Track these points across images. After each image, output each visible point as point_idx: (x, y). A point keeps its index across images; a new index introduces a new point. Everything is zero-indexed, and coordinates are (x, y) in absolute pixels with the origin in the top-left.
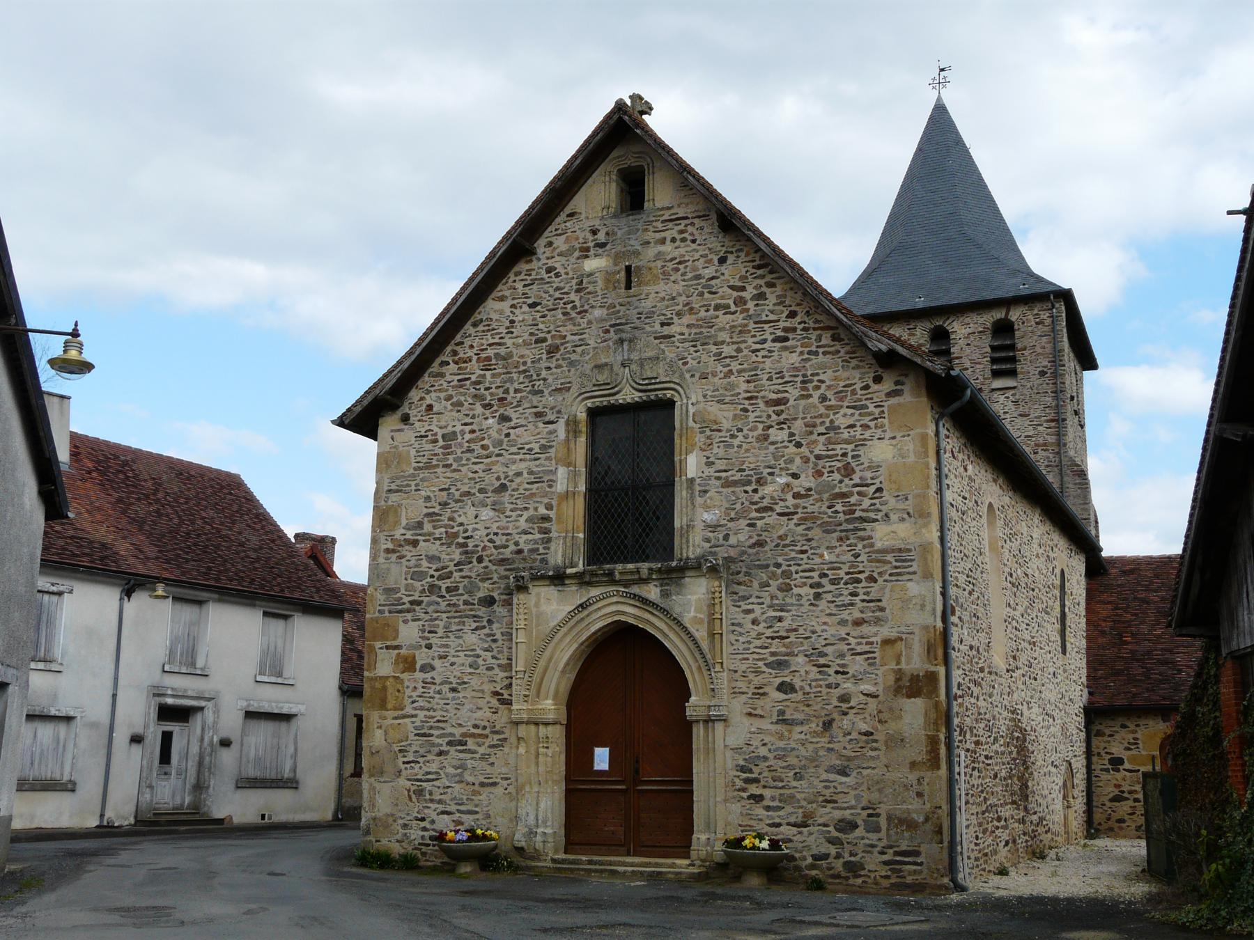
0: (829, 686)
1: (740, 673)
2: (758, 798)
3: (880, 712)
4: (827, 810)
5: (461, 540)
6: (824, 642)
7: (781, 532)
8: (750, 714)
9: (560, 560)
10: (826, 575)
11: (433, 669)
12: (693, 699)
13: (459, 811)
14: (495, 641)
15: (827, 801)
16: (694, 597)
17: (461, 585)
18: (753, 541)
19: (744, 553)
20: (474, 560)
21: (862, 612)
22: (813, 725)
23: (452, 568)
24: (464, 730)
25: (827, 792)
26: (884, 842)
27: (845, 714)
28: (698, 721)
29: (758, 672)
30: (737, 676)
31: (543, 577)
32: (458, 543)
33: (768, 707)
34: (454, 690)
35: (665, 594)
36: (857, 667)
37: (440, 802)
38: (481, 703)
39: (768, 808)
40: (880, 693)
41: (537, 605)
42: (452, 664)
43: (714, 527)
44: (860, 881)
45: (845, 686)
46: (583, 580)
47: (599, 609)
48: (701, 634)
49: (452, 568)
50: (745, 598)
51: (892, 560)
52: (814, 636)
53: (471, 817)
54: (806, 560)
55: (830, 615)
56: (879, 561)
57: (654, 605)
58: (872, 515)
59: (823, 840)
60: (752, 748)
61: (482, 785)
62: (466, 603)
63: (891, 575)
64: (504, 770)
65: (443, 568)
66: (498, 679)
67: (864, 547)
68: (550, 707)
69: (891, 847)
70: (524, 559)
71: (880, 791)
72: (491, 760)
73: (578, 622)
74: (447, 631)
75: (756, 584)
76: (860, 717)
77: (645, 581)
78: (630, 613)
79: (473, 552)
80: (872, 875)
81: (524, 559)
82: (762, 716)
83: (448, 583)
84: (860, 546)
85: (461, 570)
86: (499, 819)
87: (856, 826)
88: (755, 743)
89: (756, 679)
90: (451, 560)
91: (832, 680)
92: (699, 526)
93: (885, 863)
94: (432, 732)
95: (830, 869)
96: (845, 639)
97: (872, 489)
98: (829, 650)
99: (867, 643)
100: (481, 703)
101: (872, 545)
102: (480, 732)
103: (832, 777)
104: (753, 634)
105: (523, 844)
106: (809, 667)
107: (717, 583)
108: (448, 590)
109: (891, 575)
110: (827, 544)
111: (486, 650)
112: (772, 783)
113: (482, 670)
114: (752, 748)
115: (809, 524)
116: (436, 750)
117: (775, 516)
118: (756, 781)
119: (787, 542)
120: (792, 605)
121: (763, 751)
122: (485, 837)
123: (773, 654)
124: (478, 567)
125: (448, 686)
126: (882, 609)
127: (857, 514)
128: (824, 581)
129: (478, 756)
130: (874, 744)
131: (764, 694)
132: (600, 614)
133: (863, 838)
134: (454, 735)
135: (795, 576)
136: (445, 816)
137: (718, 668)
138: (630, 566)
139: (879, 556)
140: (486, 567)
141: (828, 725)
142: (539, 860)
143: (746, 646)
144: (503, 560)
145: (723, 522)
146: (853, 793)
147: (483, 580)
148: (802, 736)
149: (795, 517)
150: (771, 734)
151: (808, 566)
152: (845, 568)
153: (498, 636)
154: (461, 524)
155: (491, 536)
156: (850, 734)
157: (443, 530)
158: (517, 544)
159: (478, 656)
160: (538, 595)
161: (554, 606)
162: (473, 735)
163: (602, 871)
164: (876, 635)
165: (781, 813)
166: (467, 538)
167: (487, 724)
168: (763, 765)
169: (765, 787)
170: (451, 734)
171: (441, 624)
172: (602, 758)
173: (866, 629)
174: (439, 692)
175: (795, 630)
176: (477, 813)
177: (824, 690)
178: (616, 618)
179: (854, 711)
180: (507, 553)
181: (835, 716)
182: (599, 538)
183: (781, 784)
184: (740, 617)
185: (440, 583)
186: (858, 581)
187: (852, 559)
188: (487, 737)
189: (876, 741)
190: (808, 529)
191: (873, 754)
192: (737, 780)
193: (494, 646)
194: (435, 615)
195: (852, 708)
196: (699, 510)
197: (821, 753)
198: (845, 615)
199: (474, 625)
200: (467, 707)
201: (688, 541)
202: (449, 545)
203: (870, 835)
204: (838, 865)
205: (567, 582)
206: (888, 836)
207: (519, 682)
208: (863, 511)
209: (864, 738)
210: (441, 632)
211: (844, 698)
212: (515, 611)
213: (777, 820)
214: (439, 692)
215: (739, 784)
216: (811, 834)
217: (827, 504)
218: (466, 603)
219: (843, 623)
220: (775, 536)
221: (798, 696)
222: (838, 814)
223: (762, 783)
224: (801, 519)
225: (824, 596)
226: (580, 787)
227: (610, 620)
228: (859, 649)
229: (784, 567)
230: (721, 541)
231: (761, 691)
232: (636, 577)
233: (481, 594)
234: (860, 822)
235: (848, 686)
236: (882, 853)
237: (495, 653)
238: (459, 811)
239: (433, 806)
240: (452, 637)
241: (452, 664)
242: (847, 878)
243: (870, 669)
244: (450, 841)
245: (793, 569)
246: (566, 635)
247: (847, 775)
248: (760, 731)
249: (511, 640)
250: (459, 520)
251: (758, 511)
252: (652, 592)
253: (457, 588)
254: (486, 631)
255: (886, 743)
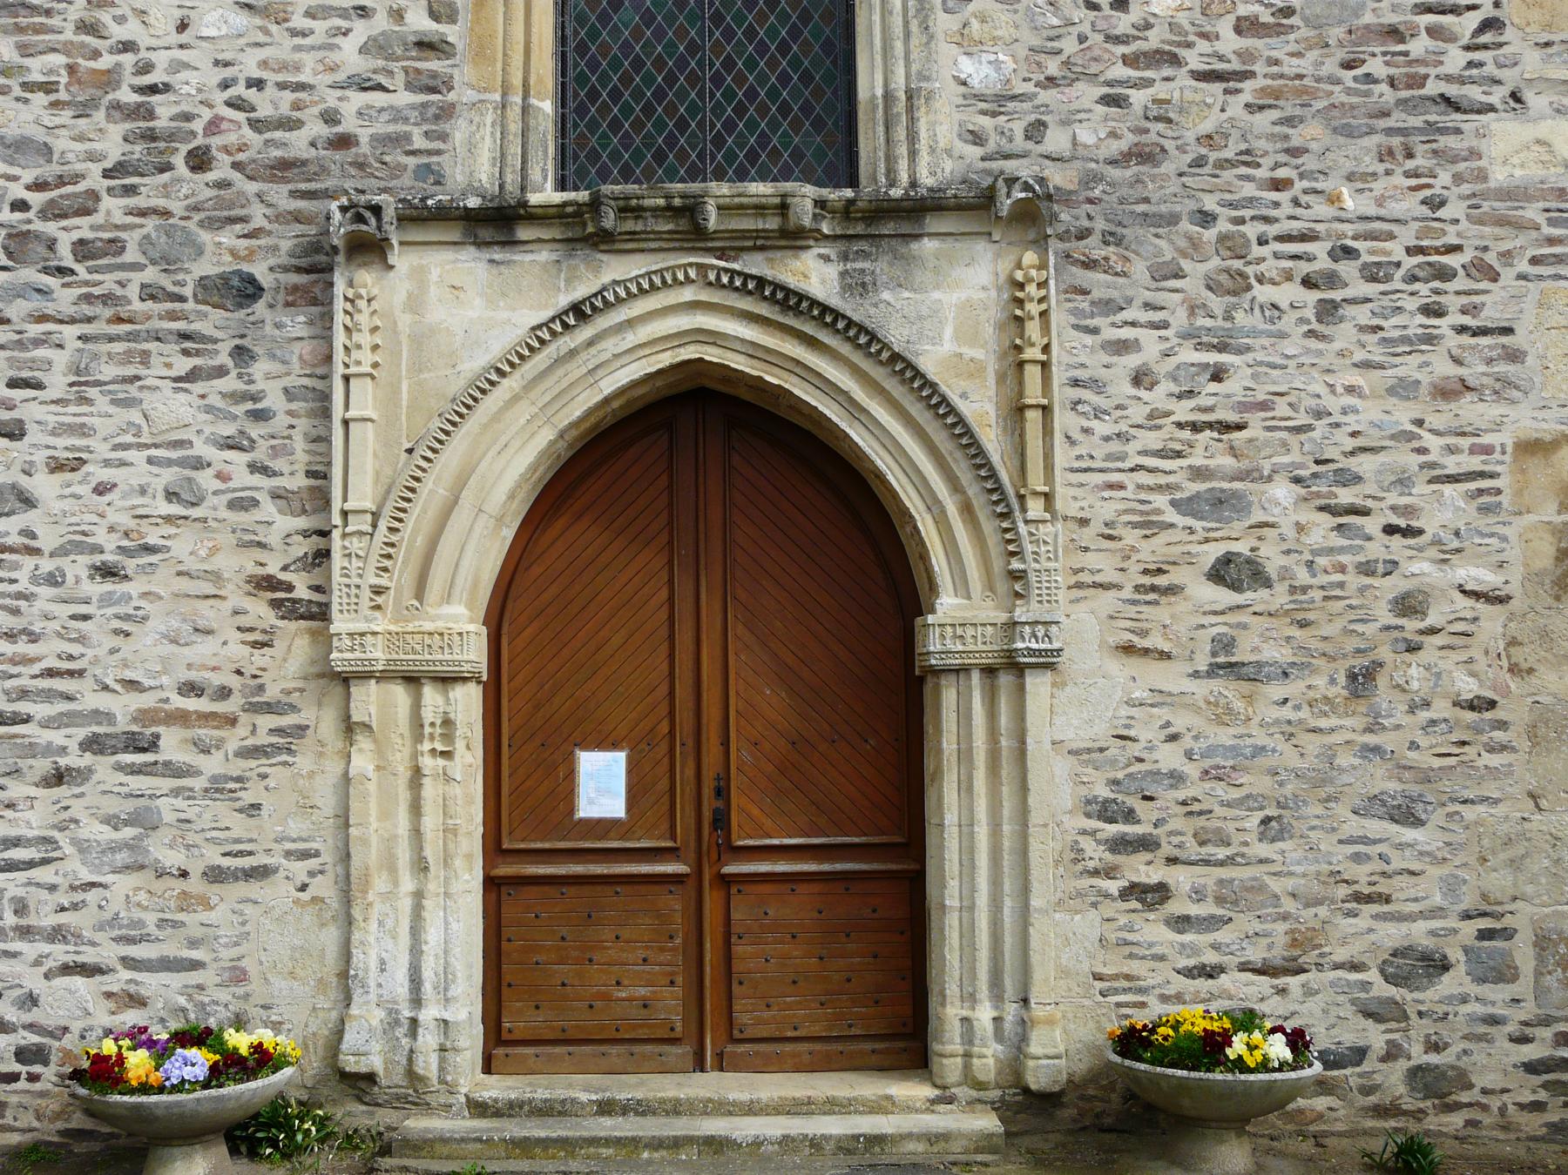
0: (1367, 569)
1: (1096, 527)
2: (1151, 895)
3: (1513, 642)
4: (1362, 923)
5: (127, 96)
6: (1350, 444)
7: (1207, 127)
8: (1128, 649)
9: (485, 174)
10: (1349, 253)
11: (28, 502)
12: (947, 604)
13: (129, 963)
14: (260, 416)
15: (1358, 898)
16: (946, 304)
17: (132, 239)
18: (1123, 145)
19: (1097, 178)
20: (179, 161)
21: (1458, 361)
22: (1320, 681)
23: (94, 180)
24: (147, 701)
25: (1361, 872)
26: (1528, 1010)
27: (1413, 648)
28: (962, 671)
29: (1150, 525)
30: (1087, 536)
31: (442, 215)
32: (117, 106)
33: (1182, 629)
34: (107, 572)
35: (857, 285)
36: (1446, 516)
37: (57, 934)
38: (208, 613)
39: (1182, 923)
40: (1514, 588)
41: (415, 304)
42: (101, 489)
43: (999, 102)
44: (1456, 1120)
45: (1415, 567)
46: (583, 231)
47: (630, 323)
48: (980, 406)
49: (94, 180)
50: (1109, 307)
51: (1541, 219)
52: (1321, 426)
53: (176, 980)
54: (1287, 209)
55: (1366, 365)
56: (1502, 222)
57: (825, 314)
58: (1475, 93)
59: (1348, 1011)
60: (1135, 749)
61: (215, 875)
62: (150, 293)
63: (1534, 261)
64: (295, 827)
65: (61, 181)
66: (274, 539)
67: (1458, 179)
68: (458, 625)
69: (1546, 1021)
70: (361, 166)
71: (1515, 864)
72: (248, 797)
73: (558, 362)
74: (82, 381)
75: (1139, 269)
76: (1456, 656)
77: (793, 238)
78: (739, 341)
79: (171, 137)
80: (1495, 1103)
81: (361, 166)
82: (1165, 656)
83: (83, 228)
84: (1444, 178)
85: (130, 190)
86: (280, 984)
87: (1445, 967)
88: (1146, 733)
89: (1145, 546)
90: (92, 157)
91: (1377, 549)
92: (947, 95)
93: (1531, 1068)
94: (24, 707)
95: (1367, 1091)
96: (1411, 436)
97: (1472, 20)
98: (1365, 465)
99: (1473, 450)
100: (208, 613)
101: (1482, 176)
102: (207, 704)
103: (1376, 827)
104: (1137, 413)
105: (376, 1063)
106: (1308, 516)
107: (1030, 257)
108: (82, 249)
109: (1534, 261)
110: (1349, 166)
111: (230, 445)
112: (1193, 850)
113: (213, 508)
114: (1135, 749)
115: (1290, 110)
116: (43, 766)
117: (1184, 80)
118: (1146, 844)
119: (1229, 154)
120: (1254, 333)
121: (1169, 758)
122: (263, 1060)
123: (1198, 473)
124: (192, 186)
125: (84, 560)
126: (1515, 356)
127: (1432, 88)
128: (1347, 269)
129: (198, 783)
130: (1498, 735)
131: (1171, 590)
132: (631, 339)
133: (1464, 1000)
134: (109, 718)
135: (1257, 251)
136: (78, 982)
137: (1035, 508)
138: (760, 189)
139: (1501, 207)
140: (223, 184)
141: (1361, 680)
142: (426, 1108)
143: (1115, 447)
144: (285, 165)
145: (1020, 88)
146: (1434, 872)
147: (212, 224)
148: (1287, 712)
149: (1248, 85)
150: (1197, 710)
151: (1296, 226)
152: (1407, 236)
153: (274, 400)
154: (128, 47)
155: (239, 90)
156: (1427, 704)
157: (59, 60)
158: (330, 118)
159: (199, 464)
160: (419, 274)
161: (474, 309)
162: (181, 718)
163: (676, 1143)
164: (1498, 426)
165: (1223, 935)
166: (153, 89)
167: (234, 682)
168: (1169, 797)
169: (1173, 861)
170: (97, 715)
171: (60, 359)
172: (602, 783)
173: (1469, 410)
174: (53, 580)
175: (1264, 406)
176: (195, 965)
177: (1354, 580)
178: (689, 353)
179: (1438, 640)
180: (298, 143)
181: (1384, 653)
182: (593, 126)
183: (1221, 853)
184: (1095, 363)
185: (50, 228)
186: (1445, 274)
187: (1425, 211)
188: (232, 721)
189: (1502, 725)
190: (1289, 121)
191: (1494, 760)
192: (1088, 845)
193: (255, 431)
194: (35, 330)
195: (1433, 631)
196: (945, 50)
197: (1345, 759)
198: (1408, 367)
199: (184, 365)
200: (156, 625)
201: (912, 137)
202: (84, 110)
203: (1486, 990)
204: (1393, 1079)
205: (523, 233)
206: (1540, 992)
207: (356, 545)
208: (1449, 79)
209: (1470, 716)
210: (57, 383)
211: (1407, 605)
212: (340, 318)
213: (1211, 958)
214: (53, 580)
215: (1096, 853)
216: (1309, 992)
217: (1341, 55)
218: (150, 293)
219: (1403, 389)
220: (1190, 136)
221: (1279, 597)
222: (1392, 935)
223: (1166, 850)
224: (1263, 91)
225: (1349, 311)
226: (534, 880)
227: (666, 359)
228: (1452, 465)
229: (1223, 226)
230: (1020, 143)
231: (1161, 581)
232: (772, 223)
233: (206, 267)
234: (1455, 955)
235: (1420, 568)
236: (1523, 1040)
237: (260, 454)
238: (129, 963)
239: (29, 949)
240: (102, 403)
241: (101, 489)
242: (1419, 1115)
243: (1482, 522)
244: (145, 1088)
245: (1252, 230)
246: (515, 399)
247: (1419, 823)
248: (1161, 697)
249: (326, 414)
250: (119, 33)
251: (1127, 61)
252: (814, 273)
253: (116, 246)
254: (230, 383)
255: (1532, 733)
